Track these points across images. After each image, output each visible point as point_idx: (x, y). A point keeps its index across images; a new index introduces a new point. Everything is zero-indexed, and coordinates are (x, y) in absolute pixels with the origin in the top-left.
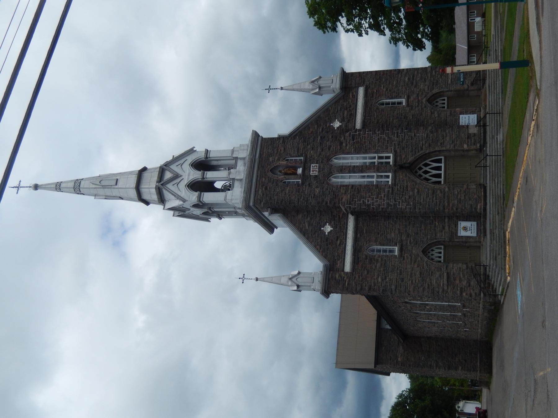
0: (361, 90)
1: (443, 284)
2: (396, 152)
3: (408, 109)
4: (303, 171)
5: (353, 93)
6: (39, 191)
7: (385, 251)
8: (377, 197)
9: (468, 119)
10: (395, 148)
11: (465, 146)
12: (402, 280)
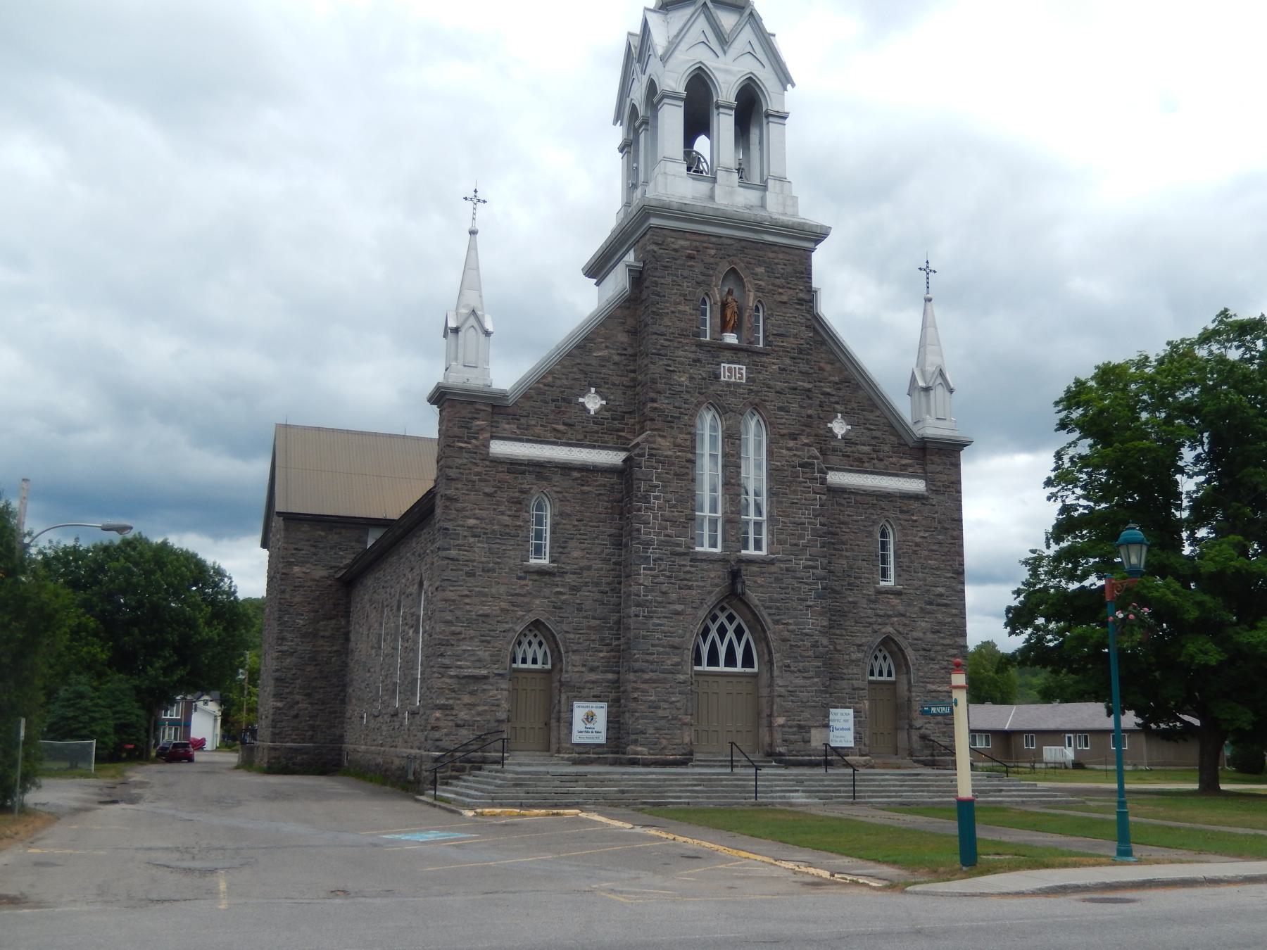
3: (871, 591)
4: (731, 347)
7: (539, 536)
9: (842, 728)
11: (781, 720)
12: (471, 574)
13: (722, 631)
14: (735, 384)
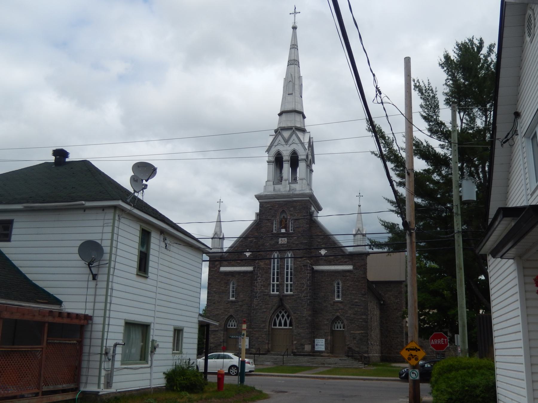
3: (332, 302)
4: (283, 233)
7: (233, 292)
8: (262, 285)
9: (320, 344)
11: (295, 342)
12: (214, 303)
13: (283, 316)
14: (283, 244)
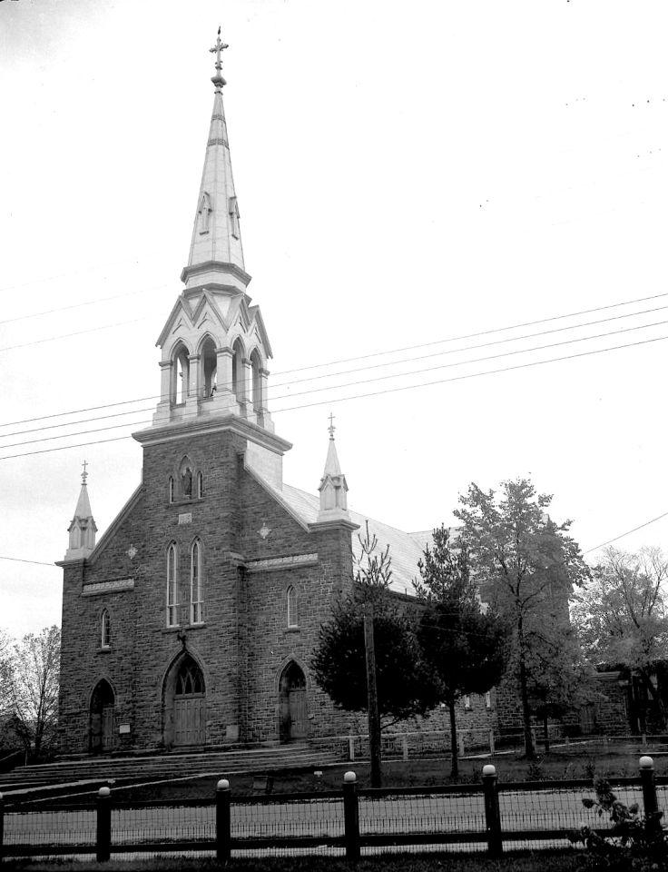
0: (313, 557)
1: (69, 709)
2: (203, 627)
5: (310, 545)
6: (213, 88)
10: (209, 625)
